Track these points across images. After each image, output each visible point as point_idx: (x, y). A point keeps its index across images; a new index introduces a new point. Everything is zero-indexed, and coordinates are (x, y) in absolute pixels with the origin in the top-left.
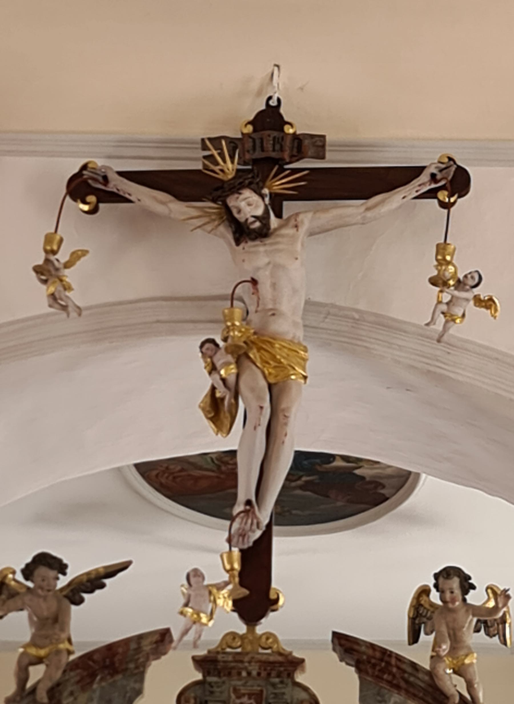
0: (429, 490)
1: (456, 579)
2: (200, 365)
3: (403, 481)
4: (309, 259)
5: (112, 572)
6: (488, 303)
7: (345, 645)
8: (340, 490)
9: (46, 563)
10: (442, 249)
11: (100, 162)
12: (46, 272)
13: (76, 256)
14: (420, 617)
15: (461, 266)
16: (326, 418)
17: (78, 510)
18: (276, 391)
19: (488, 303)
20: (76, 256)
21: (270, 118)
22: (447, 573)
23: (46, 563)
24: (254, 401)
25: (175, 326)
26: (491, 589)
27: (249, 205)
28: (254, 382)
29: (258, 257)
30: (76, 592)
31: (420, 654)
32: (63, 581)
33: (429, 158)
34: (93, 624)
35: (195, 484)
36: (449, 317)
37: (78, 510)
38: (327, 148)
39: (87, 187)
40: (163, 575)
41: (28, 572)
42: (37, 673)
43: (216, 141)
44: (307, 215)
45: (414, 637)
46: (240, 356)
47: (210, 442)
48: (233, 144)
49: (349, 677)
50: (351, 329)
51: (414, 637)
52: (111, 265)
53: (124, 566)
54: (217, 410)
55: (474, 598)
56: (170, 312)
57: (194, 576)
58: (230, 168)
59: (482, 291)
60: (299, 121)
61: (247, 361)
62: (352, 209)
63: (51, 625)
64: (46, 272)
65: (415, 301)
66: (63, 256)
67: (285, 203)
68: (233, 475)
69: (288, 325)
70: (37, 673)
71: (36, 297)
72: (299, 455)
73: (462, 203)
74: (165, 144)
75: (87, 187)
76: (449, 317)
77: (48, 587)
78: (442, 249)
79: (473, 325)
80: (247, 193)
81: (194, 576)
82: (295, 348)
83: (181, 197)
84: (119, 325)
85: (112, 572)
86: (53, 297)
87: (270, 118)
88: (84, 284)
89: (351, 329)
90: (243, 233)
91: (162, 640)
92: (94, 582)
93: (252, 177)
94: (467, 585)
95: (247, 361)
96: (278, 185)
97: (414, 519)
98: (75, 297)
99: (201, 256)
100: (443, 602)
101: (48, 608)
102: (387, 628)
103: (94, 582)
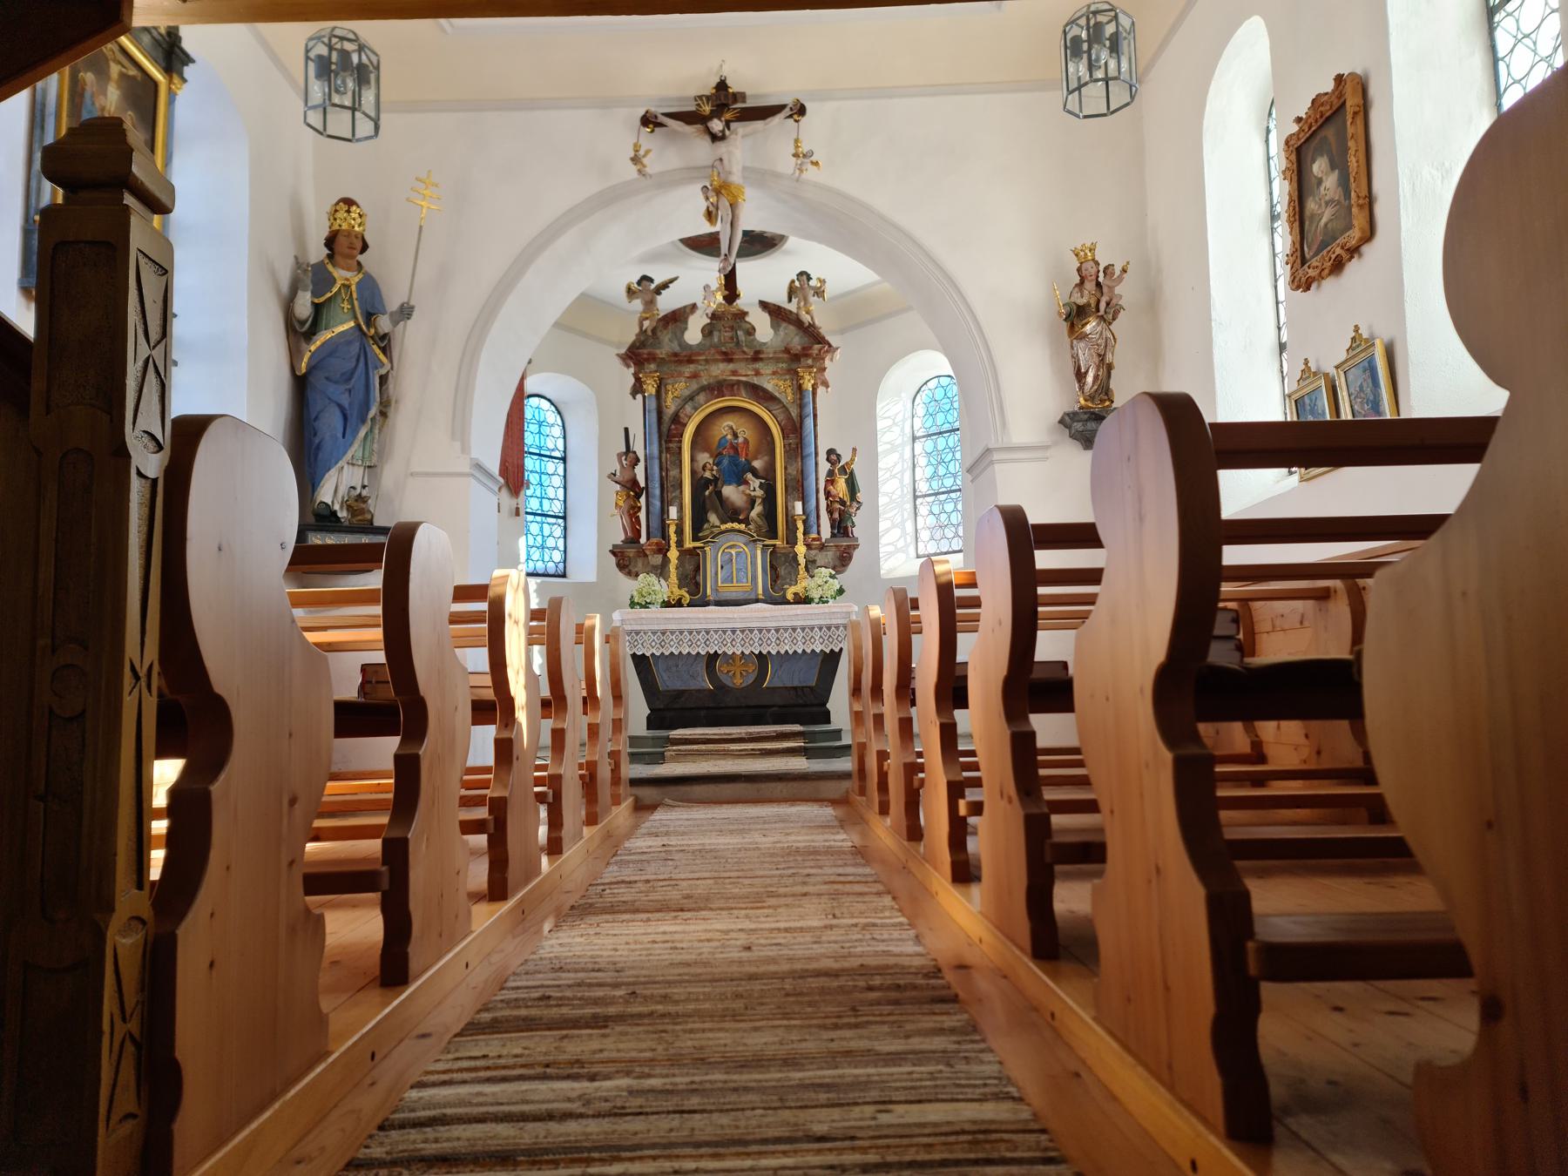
0: (792, 242)
1: (804, 275)
2: (701, 197)
3: (782, 238)
4: (745, 147)
5: (671, 281)
6: (816, 164)
7: (764, 305)
8: (759, 243)
9: (646, 279)
10: (797, 141)
11: (653, 109)
12: (636, 160)
13: (647, 152)
14: (792, 292)
15: (804, 148)
16: (753, 218)
17: (656, 257)
18: (733, 206)
19: (816, 164)
20: (647, 152)
21: (722, 86)
22: (802, 274)
23: (646, 279)
24: (724, 211)
25: (692, 180)
26: (819, 280)
27: (717, 125)
28: (724, 203)
29: (722, 148)
30: (658, 291)
31: (792, 307)
32: (653, 286)
33: (788, 100)
34: (667, 303)
35: (704, 245)
36: (801, 170)
37: (656, 257)
38: (382, 645)
39: (648, 121)
40: (695, 282)
41: (639, 283)
42: (646, 324)
43: (700, 97)
44: (740, 128)
45: (790, 300)
46: (718, 193)
47: (706, 228)
48: (708, 98)
49: (766, 317)
50: (762, 177)
51: (790, 300)
52: (665, 154)
53: (626, 430)
54: (710, 216)
55: (812, 283)
56: (688, 174)
57: (706, 287)
58: (707, 109)
59: (814, 159)
60: (734, 87)
61: (721, 194)
62: (759, 124)
63: (650, 304)
64: (636, 160)
65: (787, 164)
66: (642, 152)
67: (1269, 991)
68: (718, 240)
69: (736, 178)
70: (646, 324)
71: (632, 170)
72: (745, 233)
73: (804, 120)
74: (681, 99)
75: (648, 121)
76: (801, 170)
77: (645, 289)
78: (797, 141)
79: (811, 173)
80: (716, 121)
81: (706, 287)
82: (739, 188)
83: (688, 123)
84: (667, 182)
85: (671, 281)
86: (639, 171)
87: (722, 86)
88: (652, 164)
89: (762, 177)
90: (715, 138)
91: (694, 307)
92: (665, 286)
93: (719, 110)
94: (809, 278)
95: (721, 194)
96: (728, 116)
97: (788, 253)
98: (648, 170)
99: (700, 149)
100: (801, 285)
101: (648, 297)
102: (779, 297)
103: (665, 286)
